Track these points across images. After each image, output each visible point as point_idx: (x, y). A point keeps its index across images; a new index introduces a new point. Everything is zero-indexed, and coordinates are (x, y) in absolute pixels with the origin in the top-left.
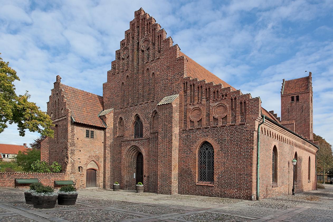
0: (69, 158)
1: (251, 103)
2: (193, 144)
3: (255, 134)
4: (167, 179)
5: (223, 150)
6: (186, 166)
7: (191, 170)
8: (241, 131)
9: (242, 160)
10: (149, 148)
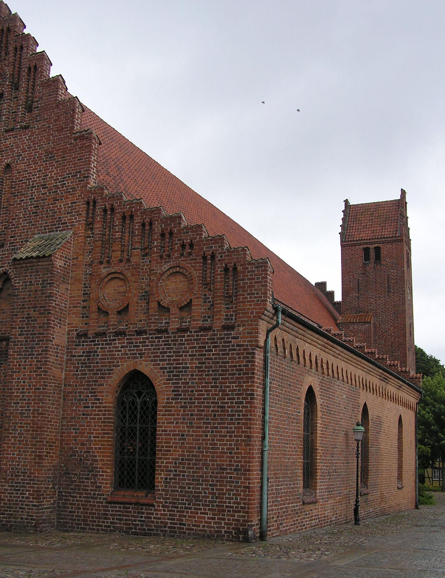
2: (104, 378)
3: (259, 356)
6: (82, 444)
8: (226, 346)
9: (227, 428)
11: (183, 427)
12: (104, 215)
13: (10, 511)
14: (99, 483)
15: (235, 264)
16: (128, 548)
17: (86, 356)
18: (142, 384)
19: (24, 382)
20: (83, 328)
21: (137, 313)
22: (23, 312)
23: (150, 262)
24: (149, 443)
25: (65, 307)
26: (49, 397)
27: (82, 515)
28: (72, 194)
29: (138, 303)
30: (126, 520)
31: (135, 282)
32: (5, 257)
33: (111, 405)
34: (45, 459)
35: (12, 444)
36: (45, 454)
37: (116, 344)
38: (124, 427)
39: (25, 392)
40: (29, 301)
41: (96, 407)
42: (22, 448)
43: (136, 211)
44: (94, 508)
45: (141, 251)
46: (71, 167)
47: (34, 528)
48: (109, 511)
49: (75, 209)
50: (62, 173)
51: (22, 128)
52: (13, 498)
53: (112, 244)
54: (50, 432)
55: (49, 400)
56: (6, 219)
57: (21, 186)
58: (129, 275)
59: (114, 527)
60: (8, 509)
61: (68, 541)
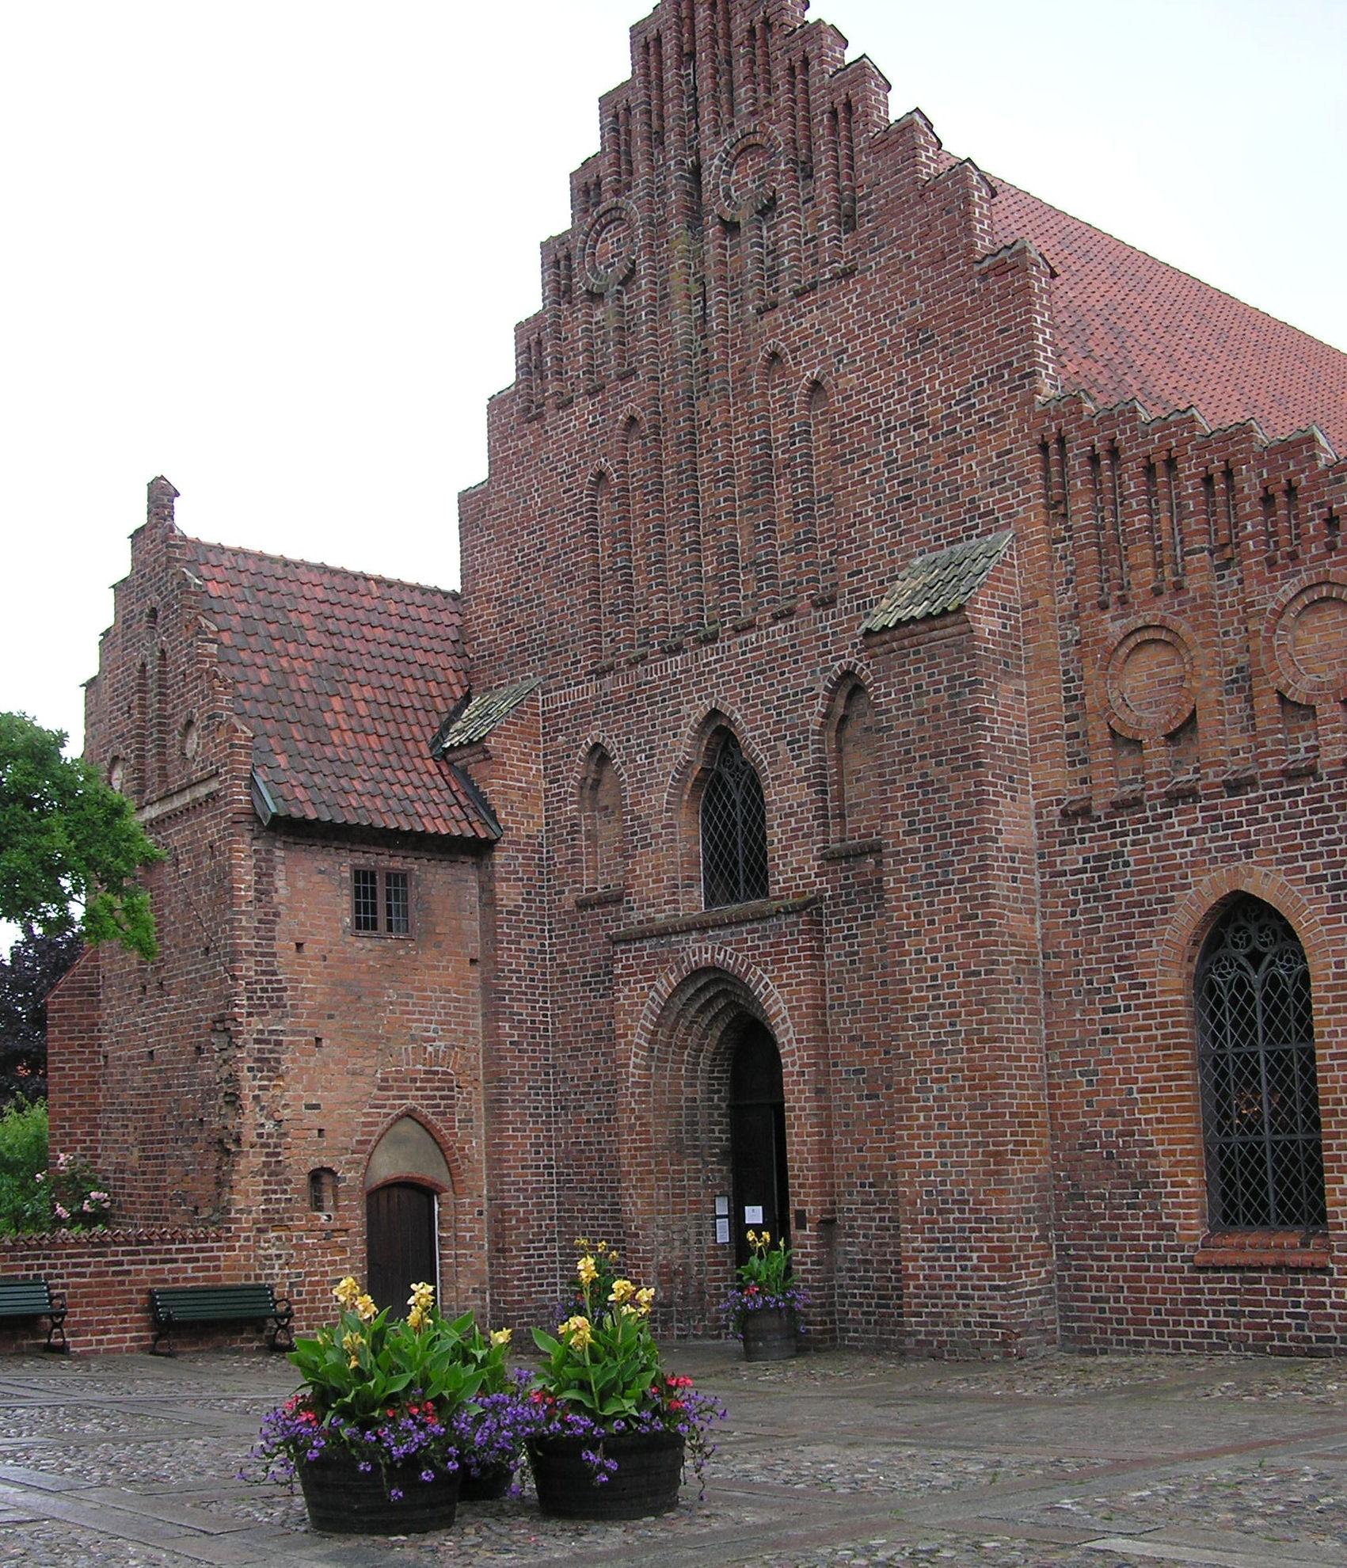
0: (248, 1103)
2: (1150, 924)
10: (823, 983)
12: (1093, 471)
13: (935, 1306)
14: (1168, 1216)
16: (1263, 1393)
17: (1094, 870)
18: (1261, 930)
19: (935, 959)
20: (1075, 792)
21: (1223, 733)
22: (908, 770)
23: (1241, 581)
24: (1298, 1094)
25: (1019, 743)
26: (1007, 992)
27: (1129, 1307)
28: (996, 431)
29: (1220, 703)
30: (1252, 1314)
31: (1204, 645)
32: (844, 631)
33: (1179, 997)
34: (1012, 1162)
35: (920, 1127)
36: (1011, 1147)
37: (1172, 825)
38: (1222, 1057)
39: (941, 987)
40: (922, 739)
42: (949, 1136)
43: (1181, 444)
44: (1160, 1286)
45: (1211, 555)
46: (984, 357)
47: (998, 1346)
48: (1201, 1291)
49: (1012, 469)
50: (960, 376)
51: (836, 277)
52: (937, 1272)
53: (1126, 548)
54: (1019, 1087)
55: (1007, 1001)
56: (831, 529)
57: (857, 435)
58: (1184, 628)
59: (1220, 1335)
60: (930, 1302)
61: (1095, 1380)
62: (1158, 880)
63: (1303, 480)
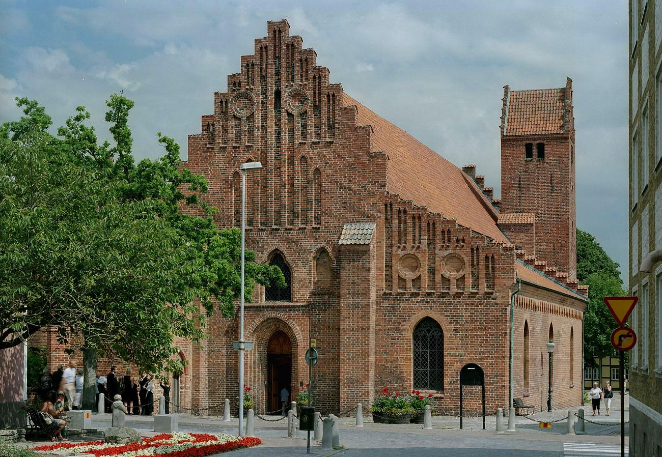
1: (502, 260)
2: (405, 321)
3: (508, 308)
4: (360, 388)
5: (460, 335)
7: (402, 370)
8: (488, 304)
9: (489, 352)
11: (462, 351)
15: (493, 255)
17: (391, 307)
19: (353, 324)
32: (322, 237)
41: (401, 339)
62: (408, 311)
63: (452, 230)
